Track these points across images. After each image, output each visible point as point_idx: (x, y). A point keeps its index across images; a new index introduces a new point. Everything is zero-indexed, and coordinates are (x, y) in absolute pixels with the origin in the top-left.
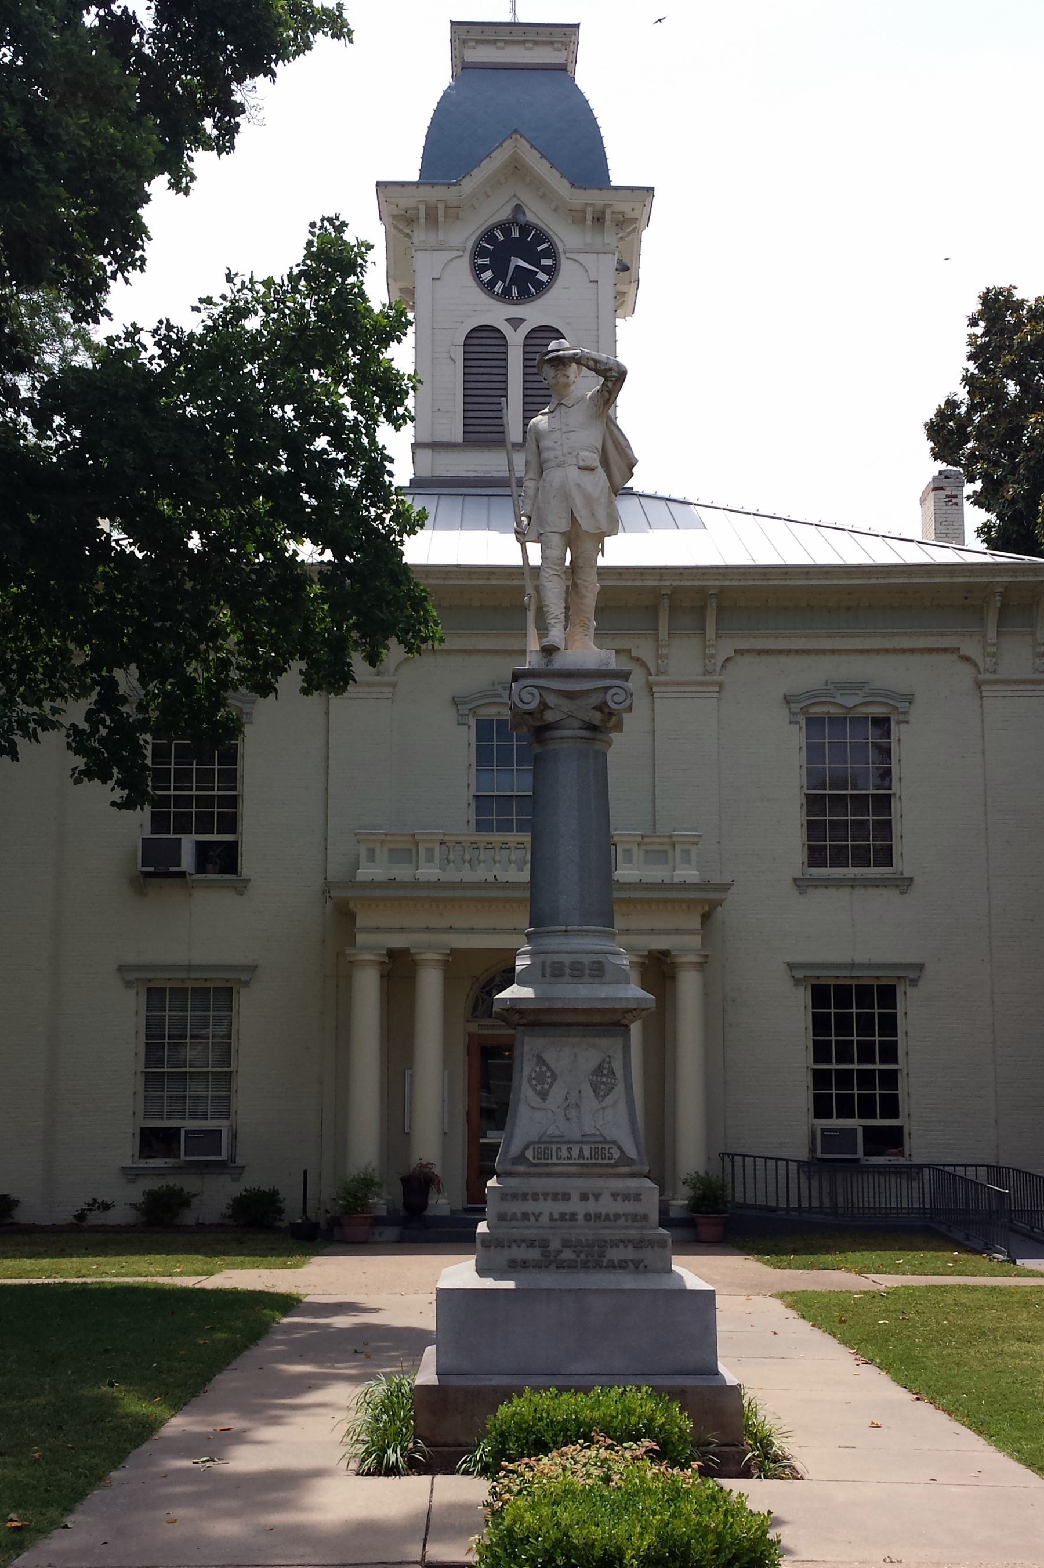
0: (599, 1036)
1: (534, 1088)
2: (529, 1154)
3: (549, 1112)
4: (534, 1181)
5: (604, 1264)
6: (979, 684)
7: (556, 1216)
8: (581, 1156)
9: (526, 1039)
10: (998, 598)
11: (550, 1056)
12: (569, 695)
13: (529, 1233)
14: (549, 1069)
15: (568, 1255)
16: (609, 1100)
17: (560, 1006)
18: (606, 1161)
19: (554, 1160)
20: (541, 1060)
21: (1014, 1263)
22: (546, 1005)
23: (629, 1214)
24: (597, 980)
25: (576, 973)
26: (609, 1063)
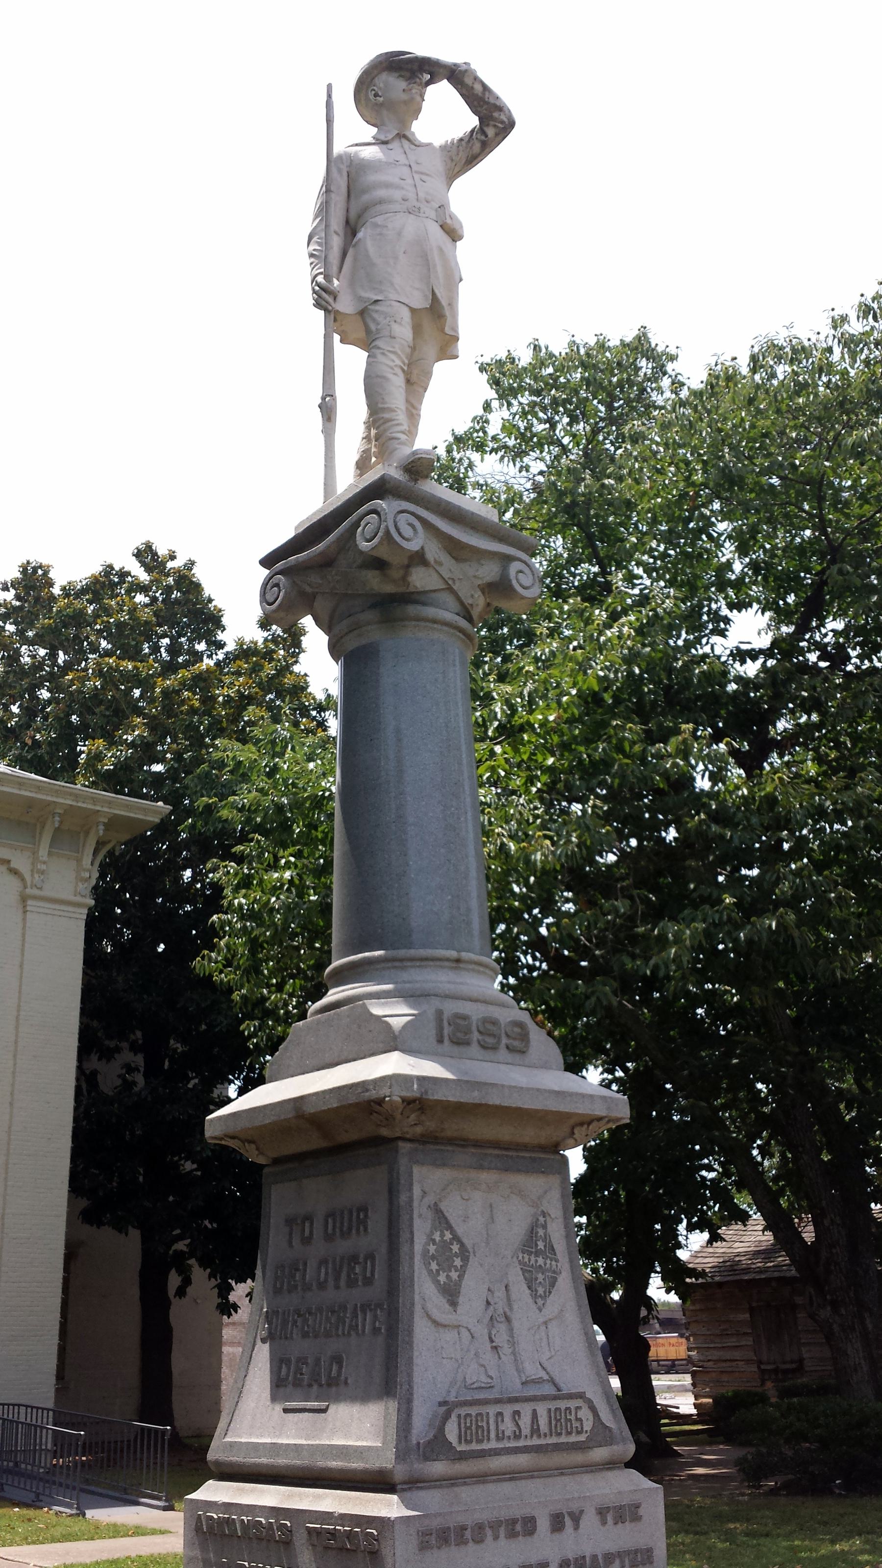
1: (434, 1276)
2: (451, 1432)
3: (465, 1334)
4: (466, 1493)
6: (24, 899)
9: (416, 1170)
10: (57, 819)
11: (452, 1208)
12: (455, 549)
14: (456, 1238)
17: (497, 1102)
18: (573, 1438)
19: (493, 1444)
20: (441, 1220)
21: (84, 1515)
22: (473, 1097)
24: (517, 1057)
25: (490, 1040)
26: (544, 1227)
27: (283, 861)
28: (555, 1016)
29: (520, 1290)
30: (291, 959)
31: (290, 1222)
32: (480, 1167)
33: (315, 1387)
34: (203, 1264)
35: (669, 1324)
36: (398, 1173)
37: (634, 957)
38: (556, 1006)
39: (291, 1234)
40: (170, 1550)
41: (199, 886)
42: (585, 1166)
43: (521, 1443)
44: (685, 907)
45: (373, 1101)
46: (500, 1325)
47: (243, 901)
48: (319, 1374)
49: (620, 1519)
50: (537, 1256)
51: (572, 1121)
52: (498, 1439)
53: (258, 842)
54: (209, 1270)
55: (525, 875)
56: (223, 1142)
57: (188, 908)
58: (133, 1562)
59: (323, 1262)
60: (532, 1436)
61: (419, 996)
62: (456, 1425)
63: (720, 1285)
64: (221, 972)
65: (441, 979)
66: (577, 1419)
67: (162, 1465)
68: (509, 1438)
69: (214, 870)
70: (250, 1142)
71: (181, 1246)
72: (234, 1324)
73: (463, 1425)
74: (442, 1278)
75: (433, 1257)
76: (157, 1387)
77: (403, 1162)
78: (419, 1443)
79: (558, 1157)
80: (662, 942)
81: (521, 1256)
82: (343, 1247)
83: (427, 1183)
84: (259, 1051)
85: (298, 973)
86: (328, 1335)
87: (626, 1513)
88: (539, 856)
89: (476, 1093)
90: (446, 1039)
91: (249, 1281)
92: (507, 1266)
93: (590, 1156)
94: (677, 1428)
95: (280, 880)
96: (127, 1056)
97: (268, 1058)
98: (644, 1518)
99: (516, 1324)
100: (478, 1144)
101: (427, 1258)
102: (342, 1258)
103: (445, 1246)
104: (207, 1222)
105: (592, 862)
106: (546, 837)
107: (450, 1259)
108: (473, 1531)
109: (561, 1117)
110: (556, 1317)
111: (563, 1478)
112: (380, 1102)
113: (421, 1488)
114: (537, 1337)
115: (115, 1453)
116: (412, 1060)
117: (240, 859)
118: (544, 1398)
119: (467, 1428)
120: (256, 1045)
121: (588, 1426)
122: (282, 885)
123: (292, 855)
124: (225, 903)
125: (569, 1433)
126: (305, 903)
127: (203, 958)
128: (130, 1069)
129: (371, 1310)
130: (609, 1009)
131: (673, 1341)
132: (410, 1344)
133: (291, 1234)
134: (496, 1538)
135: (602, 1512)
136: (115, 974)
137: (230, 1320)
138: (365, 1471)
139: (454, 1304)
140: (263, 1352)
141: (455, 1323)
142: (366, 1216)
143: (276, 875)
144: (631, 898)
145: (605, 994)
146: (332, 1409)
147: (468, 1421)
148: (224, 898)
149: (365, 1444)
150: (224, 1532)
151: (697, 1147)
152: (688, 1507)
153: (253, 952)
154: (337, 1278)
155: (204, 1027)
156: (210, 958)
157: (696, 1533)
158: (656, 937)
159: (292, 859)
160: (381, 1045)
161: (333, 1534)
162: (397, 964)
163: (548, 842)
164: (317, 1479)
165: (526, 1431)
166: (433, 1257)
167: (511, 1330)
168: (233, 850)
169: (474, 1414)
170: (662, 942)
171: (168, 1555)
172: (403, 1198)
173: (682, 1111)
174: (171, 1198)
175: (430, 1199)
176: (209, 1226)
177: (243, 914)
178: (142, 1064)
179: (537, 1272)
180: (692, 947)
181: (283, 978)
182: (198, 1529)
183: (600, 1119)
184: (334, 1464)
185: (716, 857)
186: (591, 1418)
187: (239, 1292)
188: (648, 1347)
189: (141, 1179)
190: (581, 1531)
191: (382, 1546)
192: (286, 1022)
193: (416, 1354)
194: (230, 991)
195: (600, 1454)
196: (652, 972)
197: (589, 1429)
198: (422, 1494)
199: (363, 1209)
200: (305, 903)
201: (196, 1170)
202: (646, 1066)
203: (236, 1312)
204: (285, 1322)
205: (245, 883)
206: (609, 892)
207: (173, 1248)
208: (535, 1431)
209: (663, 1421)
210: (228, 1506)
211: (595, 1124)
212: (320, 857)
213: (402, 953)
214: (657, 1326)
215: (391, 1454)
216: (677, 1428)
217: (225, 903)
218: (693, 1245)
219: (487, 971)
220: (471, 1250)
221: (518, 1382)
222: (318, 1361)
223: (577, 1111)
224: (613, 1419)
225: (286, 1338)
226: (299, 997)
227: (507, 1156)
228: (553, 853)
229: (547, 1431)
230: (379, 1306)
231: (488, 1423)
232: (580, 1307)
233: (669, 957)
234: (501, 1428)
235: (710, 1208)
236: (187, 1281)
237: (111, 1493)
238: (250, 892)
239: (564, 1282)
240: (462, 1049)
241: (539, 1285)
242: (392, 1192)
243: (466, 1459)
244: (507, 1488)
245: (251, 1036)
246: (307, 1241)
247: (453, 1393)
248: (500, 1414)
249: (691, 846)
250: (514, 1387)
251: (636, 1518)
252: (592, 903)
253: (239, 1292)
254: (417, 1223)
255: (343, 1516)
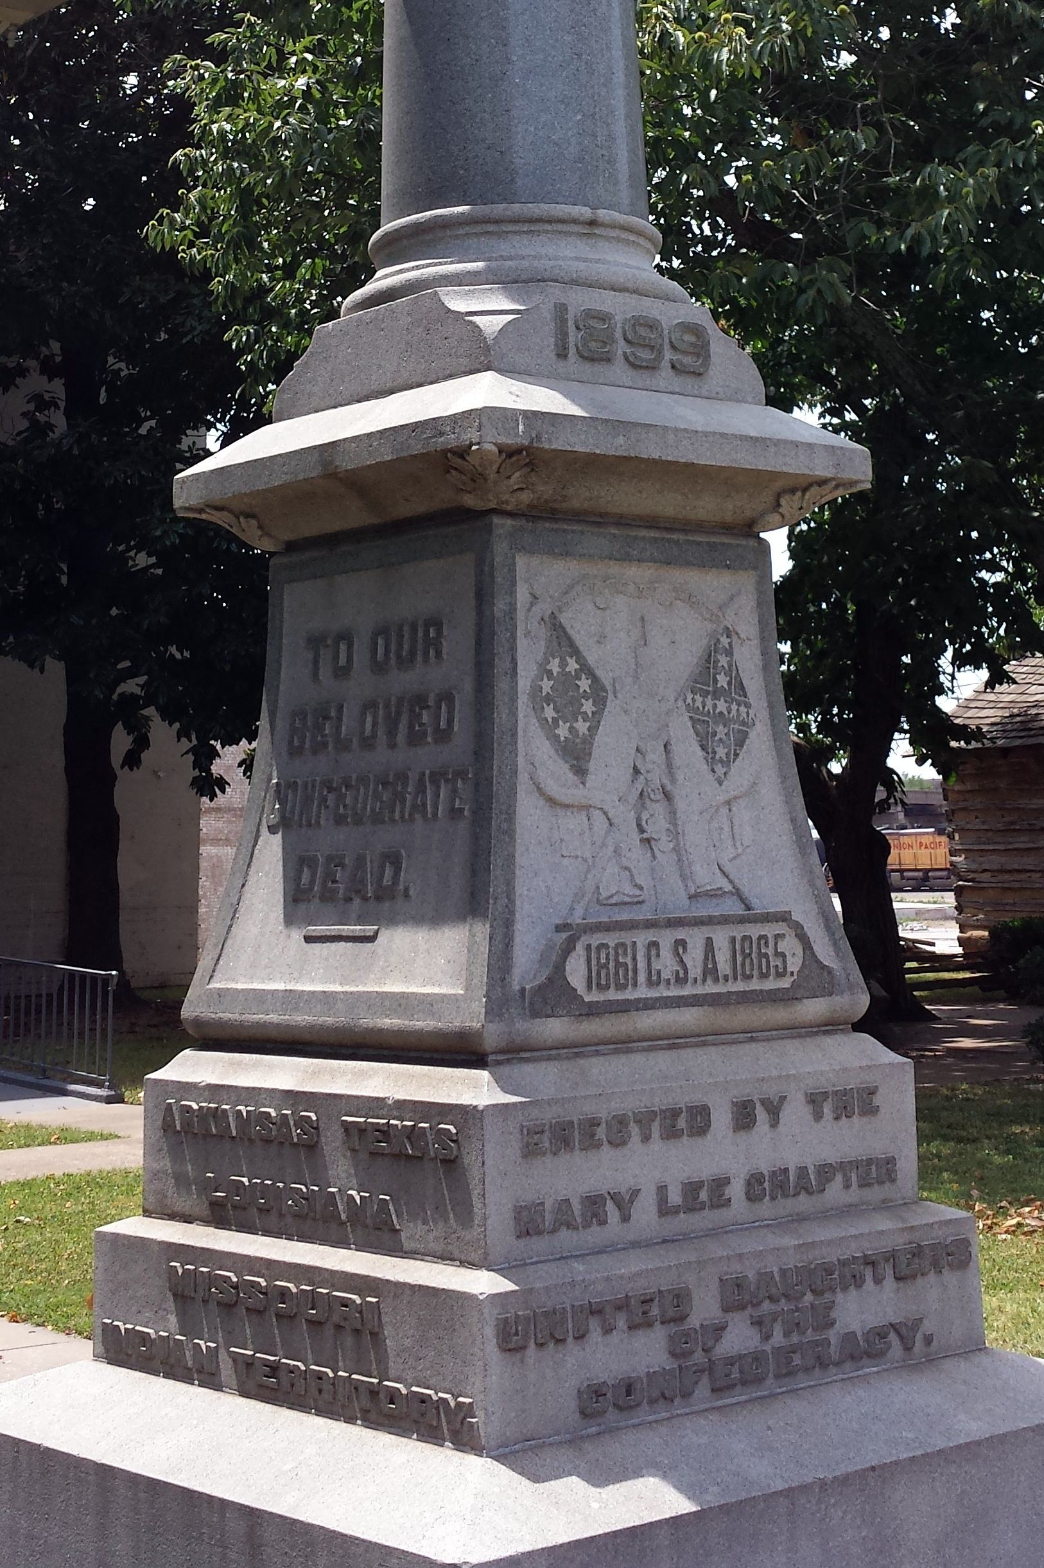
0: (702, 565)
1: (549, 728)
2: (576, 972)
3: (599, 819)
4: (599, 1068)
5: (834, 1351)
7: (675, 1197)
8: (710, 971)
9: (521, 562)
11: (581, 623)
13: (633, 1271)
14: (586, 669)
15: (739, 1337)
16: (741, 773)
18: (770, 984)
19: (643, 992)
20: (561, 639)
23: (855, 1164)
24: (689, 382)
25: (645, 355)
26: (729, 652)
27: (293, 59)
28: (744, 323)
29: (688, 750)
30: (308, 224)
31: (315, 642)
32: (626, 558)
33: (357, 901)
34: (168, 715)
35: (920, 814)
36: (492, 566)
37: (880, 224)
38: (749, 305)
39: (316, 662)
40: (119, 1165)
41: (151, 101)
42: (790, 564)
43: (687, 991)
44: (968, 142)
45: (450, 450)
46: (656, 806)
47: (228, 127)
48: (362, 881)
49: (844, 1110)
50: (716, 697)
51: (779, 485)
52: (650, 983)
53: (251, 25)
54: (177, 725)
55: (702, 86)
56: (204, 516)
57: (134, 138)
58: (57, 1184)
59: (370, 705)
60: (704, 980)
61: (526, 282)
62: (583, 960)
63: (1005, 752)
64: (191, 245)
65: (565, 253)
66: (777, 954)
67: (104, 1031)
68: (668, 981)
69: (176, 74)
70: (248, 516)
71: (132, 686)
72: (218, 810)
73: (594, 962)
74: (563, 731)
75: (548, 699)
76: (93, 910)
77: (500, 548)
78: (523, 990)
79: (752, 542)
80: (928, 198)
81: (690, 696)
82: (402, 681)
83: (537, 581)
84: (256, 375)
85: (320, 249)
86: (377, 819)
87: (854, 1102)
88: (725, 54)
89: (621, 440)
90: (572, 351)
91: (244, 742)
92: (668, 713)
93: (799, 547)
94: (931, 976)
95: (288, 91)
96: (36, 382)
97: (271, 387)
98: (882, 1111)
99: (680, 804)
100: (623, 521)
101: (538, 699)
102: (400, 701)
103: (567, 682)
104: (173, 649)
105: (814, 66)
106: (738, 22)
107: (576, 702)
108: (609, 1127)
109: (758, 479)
110: (746, 794)
111: (754, 1045)
112: (462, 452)
113: (527, 1060)
114: (715, 825)
115: (28, 1013)
116: (515, 385)
117: (219, 56)
118: (725, 920)
119: (601, 967)
120: (251, 365)
121: (794, 964)
122: (293, 100)
123: (307, 50)
124: (196, 128)
125: (764, 976)
126: (330, 131)
127: (160, 221)
128: (42, 403)
129: (447, 781)
130: (836, 309)
131: (925, 840)
132: (510, 833)
133: (316, 662)
134: (646, 1138)
135: (815, 1100)
136: (12, 248)
137: (212, 805)
138: (438, 1034)
139: (580, 772)
140: (271, 848)
141: (584, 802)
142: (439, 632)
143: (282, 83)
144: (879, 126)
145: (832, 284)
146: (384, 937)
147: (603, 955)
148: (195, 121)
149: (436, 990)
150: (208, 1129)
151: (974, 534)
152: (948, 1098)
153: (245, 212)
154: (392, 733)
155: (163, 336)
156: (172, 221)
157: (960, 1140)
158: (917, 189)
159: (309, 57)
160: (465, 361)
161: (385, 1132)
162: (491, 228)
163: (740, 30)
164: (359, 1046)
165: (695, 971)
166: (548, 699)
167: (673, 813)
168: (209, 40)
169: (612, 944)
170: (928, 198)
171: (114, 1172)
172: (500, 606)
173: (950, 475)
174: (114, 611)
175: (544, 608)
176: (178, 656)
177: (226, 148)
178: (63, 397)
179: (716, 723)
180: (978, 208)
181: (295, 256)
182: (167, 1127)
183: (822, 482)
184: (387, 1022)
185: (1023, 57)
186: (799, 951)
187: (227, 760)
188: (886, 849)
189: (64, 580)
190: (781, 1128)
191: (464, 1152)
192: (300, 328)
193: (519, 849)
194: (207, 277)
195: (814, 1008)
196: (908, 248)
197: (796, 970)
198: (528, 1068)
199: (435, 622)
200: (330, 131)
201: (153, 566)
202: (895, 403)
203: (223, 791)
204: (308, 800)
205: (231, 96)
206: (840, 116)
207: (119, 690)
208: (710, 971)
209: (908, 965)
210: (215, 1090)
211: (815, 490)
212: (356, 53)
213: (499, 209)
214: (901, 816)
215: (479, 1006)
216: (931, 976)
217: (196, 128)
218: (962, 690)
219: (641, 241)
220: (609, 688)
221: (683, 895)
222: (360, 861)
223: (785, 469)
224: (834, 954)
225: (309, 825)
226: (321, 287)
227: (669, 541)
228: (749, 48)
229: (729, 972)
230: (461, 774)
231: (634, 959)
232: (784, 778)
233: (938, 224)
234: (656, 966)
235: (992, 631)
236: (142, 742)
237: (20, 1076)
238: (239, 111)
239: (760, 739)
240: (599, 368)
241: (719, 743)
242: (483, 595)
243: (598, 1014)
244: (662, 1061)
245: (241, 352)
246: (342, 673)
247: (579, 911)
248: (655, 944)
249: (981, 39)
250: (677, 902)
251: (870, 1110)
252: (812, 135)
253: (227, 760)
254: (522, 643)
255: (401, 1104)
